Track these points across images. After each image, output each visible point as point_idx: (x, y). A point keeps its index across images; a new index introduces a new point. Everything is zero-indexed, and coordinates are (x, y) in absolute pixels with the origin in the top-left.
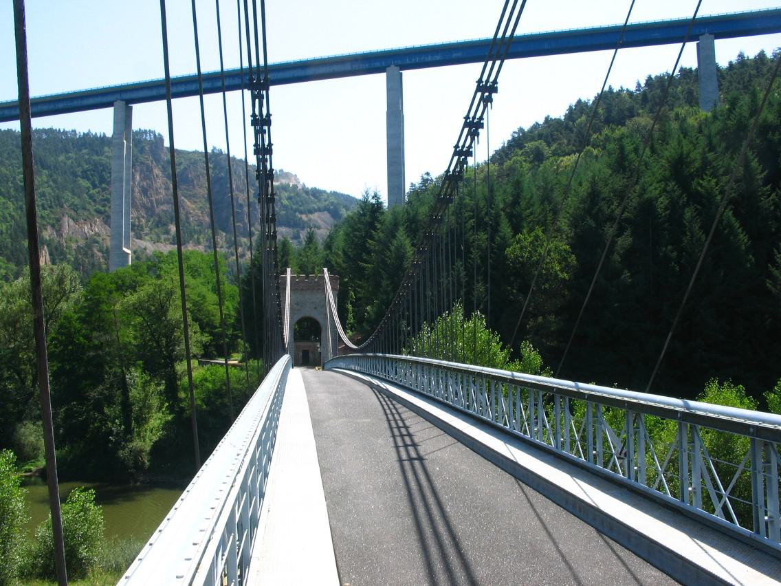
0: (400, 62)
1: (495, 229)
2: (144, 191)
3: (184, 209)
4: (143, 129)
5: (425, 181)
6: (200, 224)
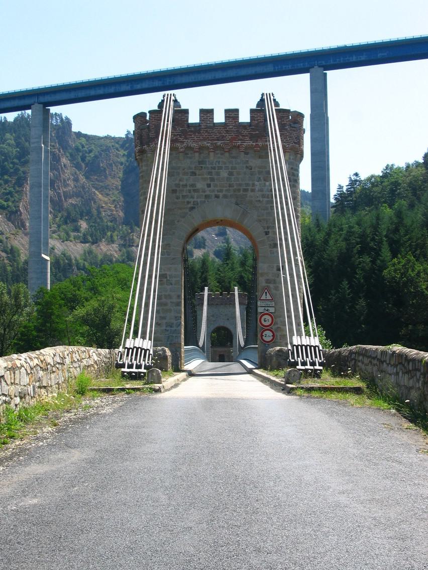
0: (324, 63)
1: (378, 252)
3: (95, 202)
5: (353, 183)
6: (114, 220)
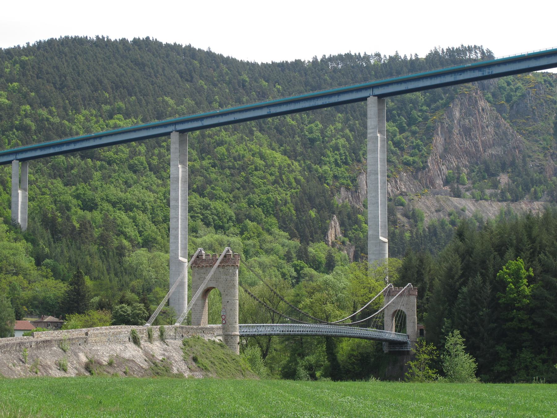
2: (467, 132)
4: (466, 45)
